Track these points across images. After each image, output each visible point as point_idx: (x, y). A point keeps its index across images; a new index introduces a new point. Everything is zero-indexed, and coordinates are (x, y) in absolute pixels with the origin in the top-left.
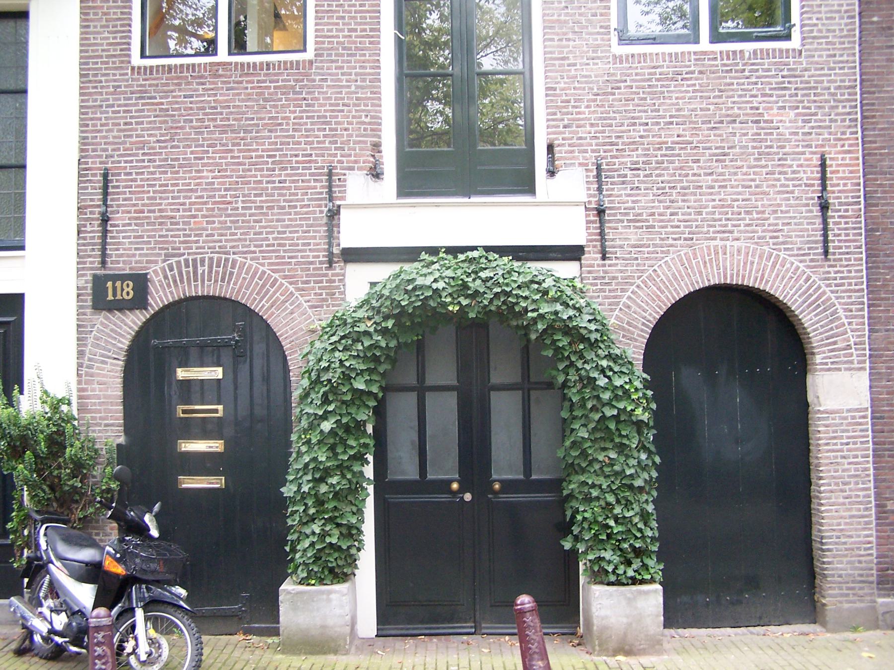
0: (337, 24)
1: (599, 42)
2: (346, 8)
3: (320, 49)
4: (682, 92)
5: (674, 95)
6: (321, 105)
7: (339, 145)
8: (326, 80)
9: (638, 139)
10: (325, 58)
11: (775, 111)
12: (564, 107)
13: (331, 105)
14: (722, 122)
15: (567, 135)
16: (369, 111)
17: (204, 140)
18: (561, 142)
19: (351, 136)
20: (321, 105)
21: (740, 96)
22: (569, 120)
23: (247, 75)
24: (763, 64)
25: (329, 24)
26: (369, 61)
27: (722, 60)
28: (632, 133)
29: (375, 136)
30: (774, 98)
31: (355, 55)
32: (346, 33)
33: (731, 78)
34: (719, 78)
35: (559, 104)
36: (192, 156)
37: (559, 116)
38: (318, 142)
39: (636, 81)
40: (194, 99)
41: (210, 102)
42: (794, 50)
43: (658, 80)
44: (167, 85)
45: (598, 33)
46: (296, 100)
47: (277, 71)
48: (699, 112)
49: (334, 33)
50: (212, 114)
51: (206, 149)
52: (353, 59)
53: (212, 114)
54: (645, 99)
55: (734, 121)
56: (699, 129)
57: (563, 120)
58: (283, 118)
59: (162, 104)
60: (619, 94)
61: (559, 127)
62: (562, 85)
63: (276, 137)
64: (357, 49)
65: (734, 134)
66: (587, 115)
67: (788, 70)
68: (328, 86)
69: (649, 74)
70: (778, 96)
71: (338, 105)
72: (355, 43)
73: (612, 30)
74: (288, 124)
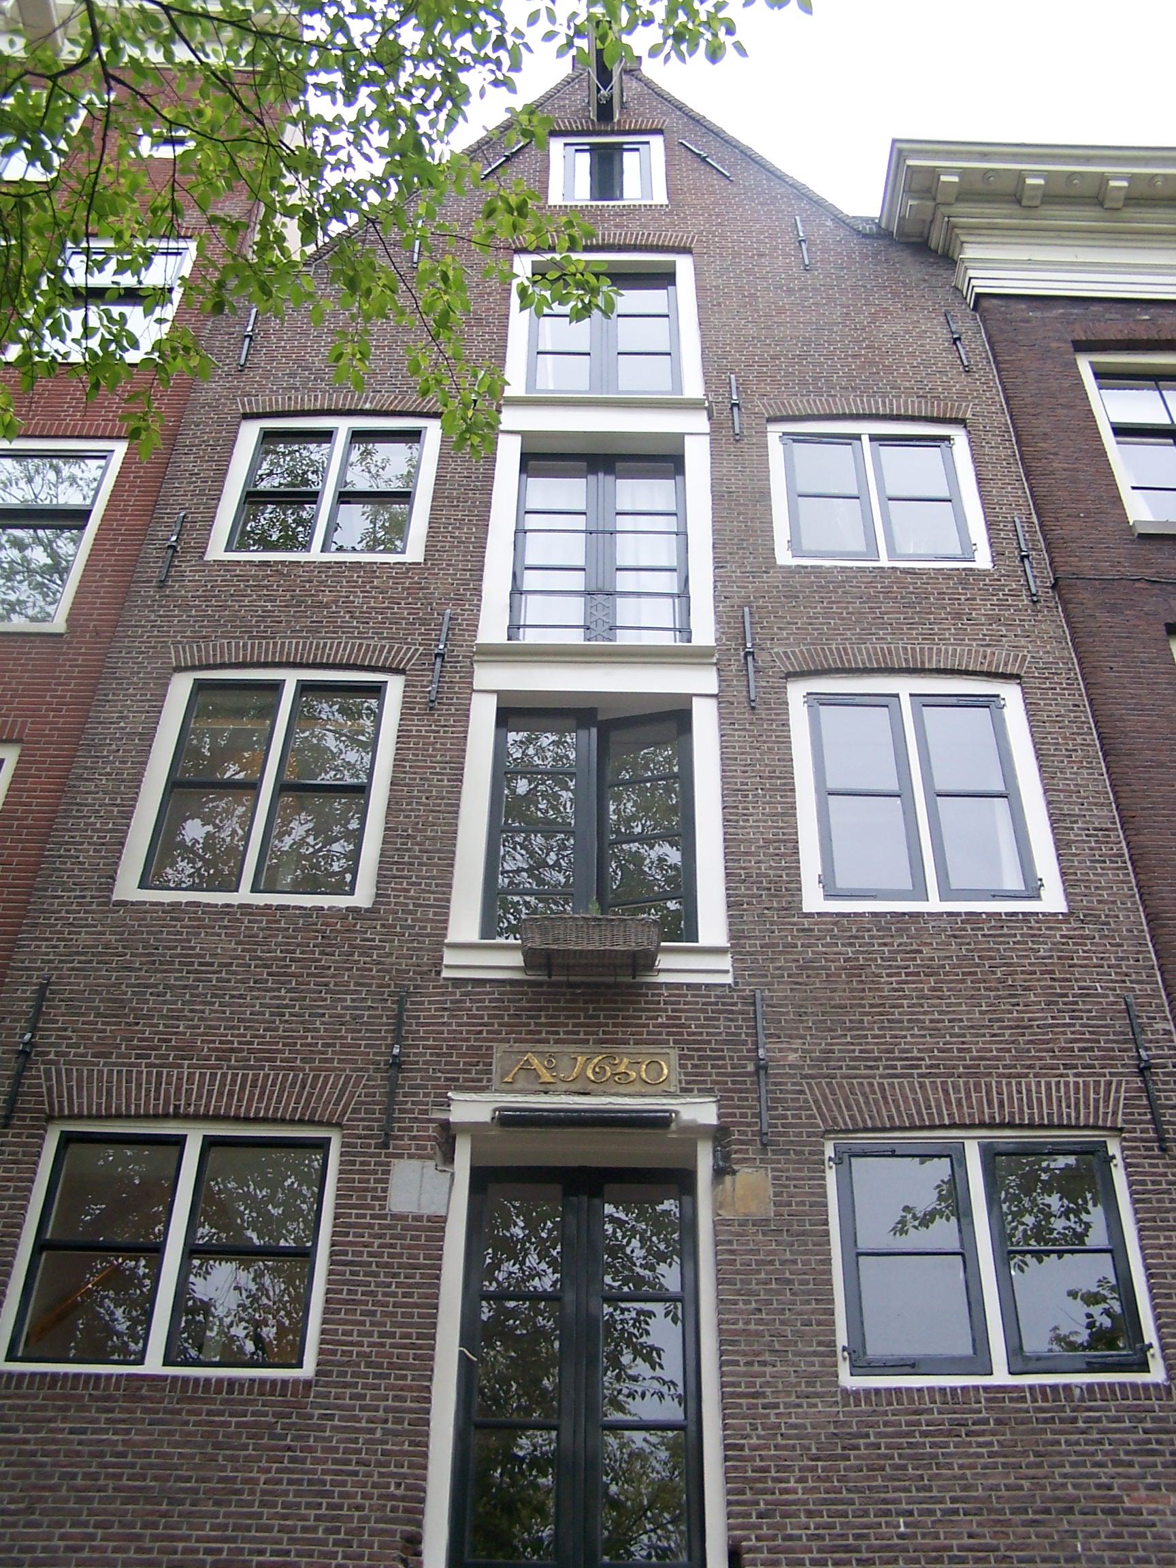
0: (363, 1323)
1: (817, 1368)
2: (380, 1297)
3: (327, 1363)
4: (969, 1456)
5: (956, 1462)
6: (316, 1461)
7: (342, 1536)
8: (331, 1417)
9: (896, 1541)
10: (334, 1378)
11: (1143, 1493)
12: (759, 1480)
13: (335, 1462)
14: (1047, 1511)
15: (765, 1531)
16: (404, 1476)
17: (91, 1513)
18: (753, 1542)
19: (366, 1519)
20: (316, 1461)
21: (1074, 1464)
22: (767, 1503)
23: (191, 1400)
24: (1108, 1409)
25: (346, 1322)
26: (411, 1389)
27: (1035, 1400)
28: (884, 1529)
29: (409, 1522)
30: (1137, 1470)
31: (388, 1376)
32: (375, 1339)
33: (1054, 1432)
34: (1033, 1432)
35: (750, 1474)
36: (62, 1543)
37: (748, 1496)
38: (305, 1529)
39: (886, 1435)
40: (89, 1437)
41: (115, 1443)
42: (1156, 1386)
43: (924, 1434)
44: (43, 1408)
45: (815, 1354)
46: (274, 1449)
47: (244, 1396)
48: (1004, 1493)
49: (355, 1338)
50: (114, 1465)
51: (91, 1530)
52: (383, 1383)
53: (114, 1465)
54: (904, 1467)
55: (1070, 1511)
56: (1007, 1523)
57: (757, 1503)
58: (245, 1481)
59: (26, 1442)
60: (856, 1458)
61: (750, 1516)
62: (754, 1441)
63: (227, 1515)
64: (391, 1366)
65: (1074, 1535)
66: (800, 1495)
67: (1153, 1420)
68: (334, 1428)
69: (908, 1424)
70: (1143, 1465)
71: (347, 1462)
72: (390, 1355)
73: (839, 1349)
74: (252, 1492)
